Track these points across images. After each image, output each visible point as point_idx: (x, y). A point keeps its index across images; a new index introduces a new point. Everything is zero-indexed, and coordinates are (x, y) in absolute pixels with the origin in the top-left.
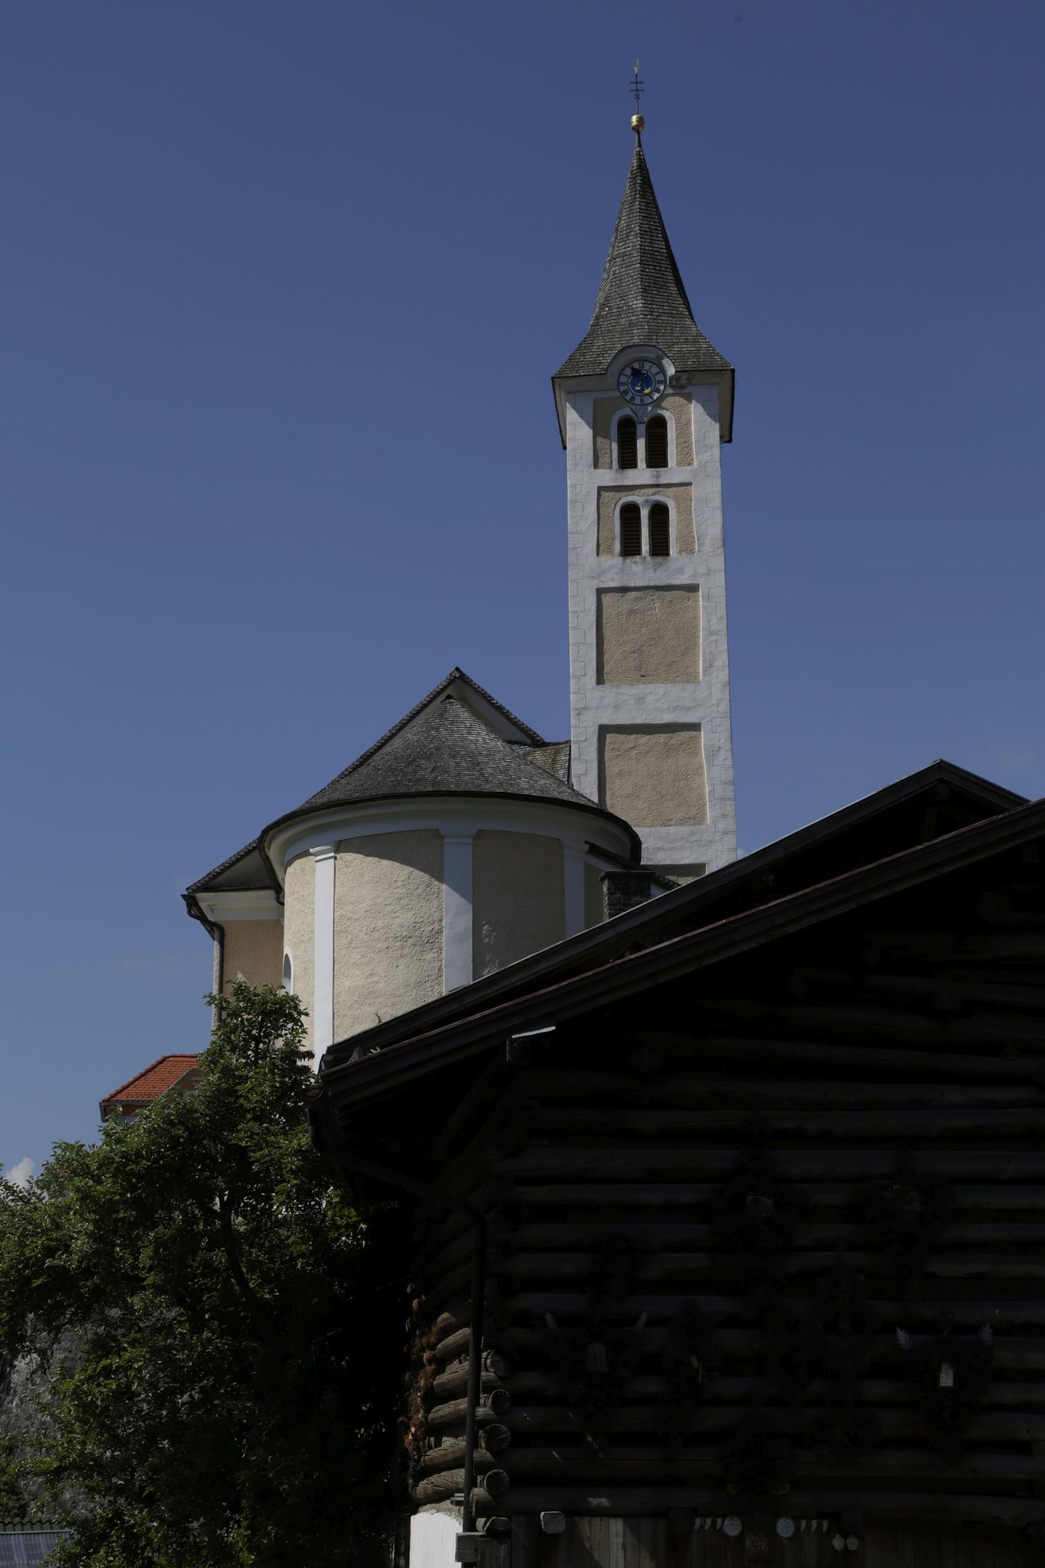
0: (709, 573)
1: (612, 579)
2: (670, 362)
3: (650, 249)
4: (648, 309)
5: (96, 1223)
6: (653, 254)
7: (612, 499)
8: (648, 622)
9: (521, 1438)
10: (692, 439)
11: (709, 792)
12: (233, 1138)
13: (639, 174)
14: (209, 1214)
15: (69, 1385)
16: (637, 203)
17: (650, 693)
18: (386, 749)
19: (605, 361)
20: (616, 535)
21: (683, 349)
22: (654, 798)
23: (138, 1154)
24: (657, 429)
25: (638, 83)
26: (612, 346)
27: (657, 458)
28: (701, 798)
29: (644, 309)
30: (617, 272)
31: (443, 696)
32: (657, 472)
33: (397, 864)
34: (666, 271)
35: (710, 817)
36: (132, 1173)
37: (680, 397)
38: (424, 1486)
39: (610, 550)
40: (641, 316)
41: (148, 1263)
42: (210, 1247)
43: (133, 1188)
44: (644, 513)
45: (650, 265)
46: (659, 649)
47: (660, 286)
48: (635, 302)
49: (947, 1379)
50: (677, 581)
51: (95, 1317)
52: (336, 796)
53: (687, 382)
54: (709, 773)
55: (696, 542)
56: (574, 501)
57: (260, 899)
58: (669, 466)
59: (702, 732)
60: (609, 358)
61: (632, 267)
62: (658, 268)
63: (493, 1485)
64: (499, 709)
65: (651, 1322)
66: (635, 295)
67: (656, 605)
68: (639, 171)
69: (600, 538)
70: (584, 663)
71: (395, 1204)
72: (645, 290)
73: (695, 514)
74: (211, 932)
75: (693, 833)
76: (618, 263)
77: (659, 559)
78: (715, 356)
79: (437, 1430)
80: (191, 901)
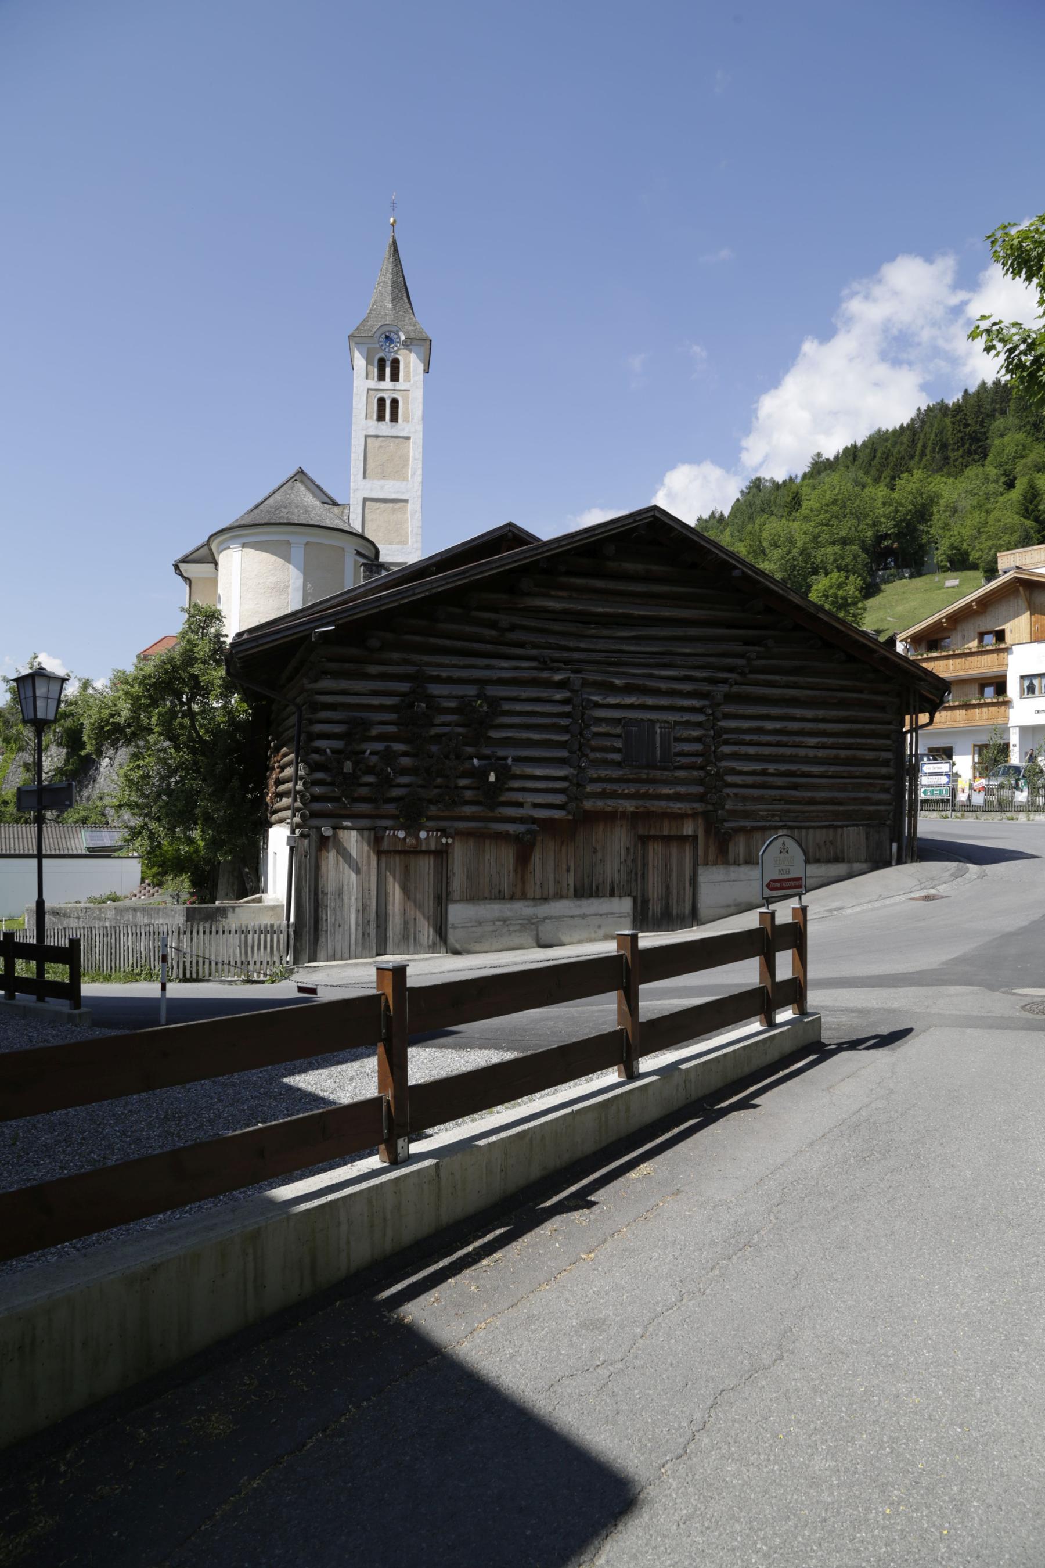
5: (132, 704)
9: (315, 798)
12: (192, 671)
14: (182, 704)
15: (122, 772)
18: (266, 502)
23: (150, 676)
24: (396, 363)
27: (395, 377)
31: (293, 480)
33: (270, 555)
36: (147, 684)
38: (275, 817)
39: (371, 418)
41: (155, 723)
42: (182, 717)
43: (148, 690)
49: (492, 778)
51: (133, 744)
52: (243, 523)
56: (356, 394)
57: (207, 568)
63: (302, 816)
64: (318, 487)
65: (371, 754)
71: (264, 702)
72: (393, 300)
74: (185, 581)
77: (394, 424)
79: (280, 795)
80: (177, 567)
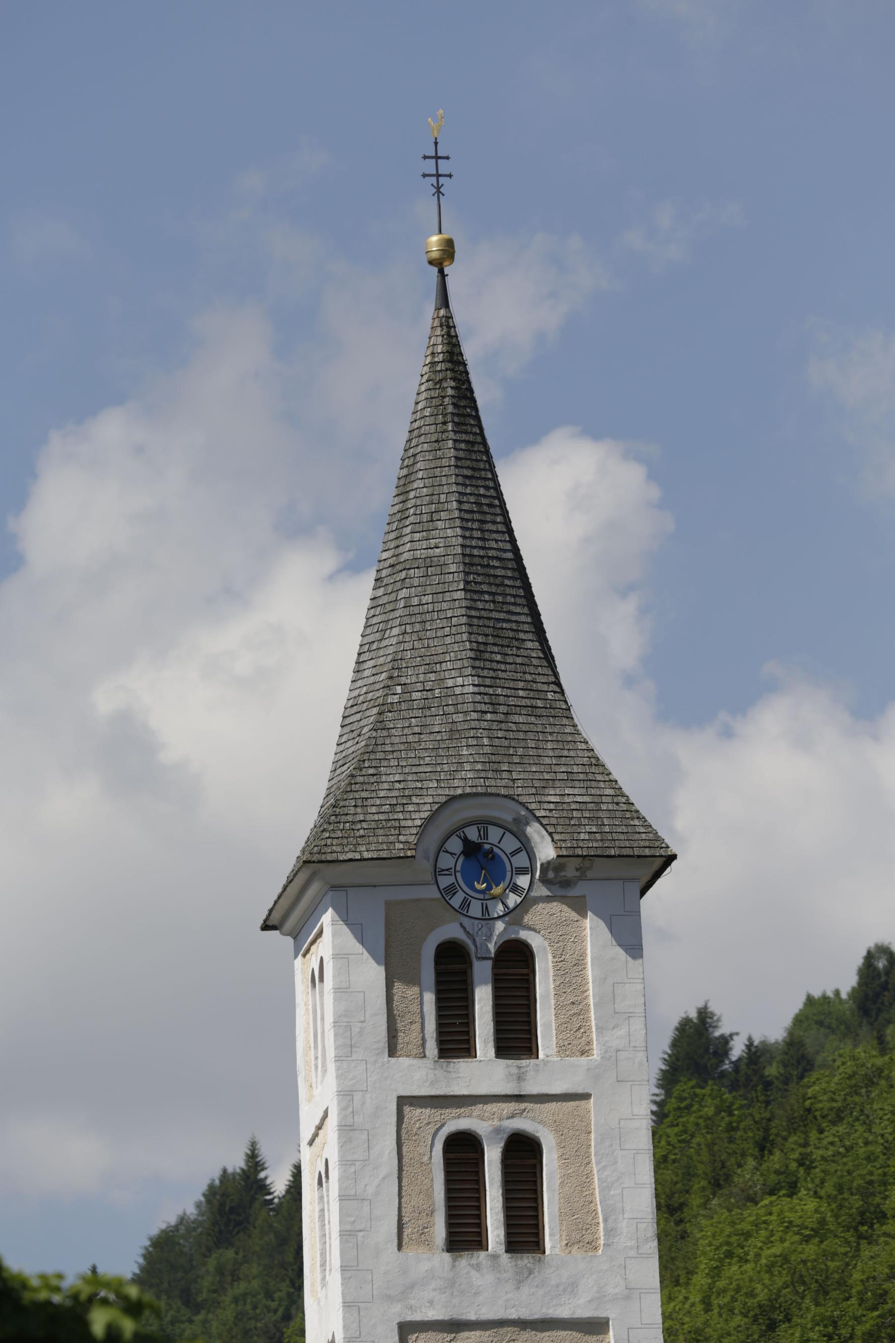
0: (630, 1293)
1: (431, 1302)
2: (544, 832)
3: (482, 553)
6: (488, 566)
7: (429, 1123)
10: (587, 997)
16: (450, 444)
19: (409, 823)
20: (437, 1206)
21: (567, 799)
25: (440, 158)
26: (419, 785)
30: (415, 601)
32: (519, 1068)
34: (515, 604)
37: (563, 903)
40: (474, 716)
44: (492, 1157)
45: (483, 592)
47: (505, 642)
48: (460, 681)
53: (578, 874)
55: (601, 1225)
58: (541, 1054)
61: (447, 597)
62: (500, 599)
66: (458, 664)
68: (449, 365)
69: (404, 1210)
72: (479, 654)
73: (598, 1163)
76: (416, 582)
77: (526, 1260)
78: (632, 819)
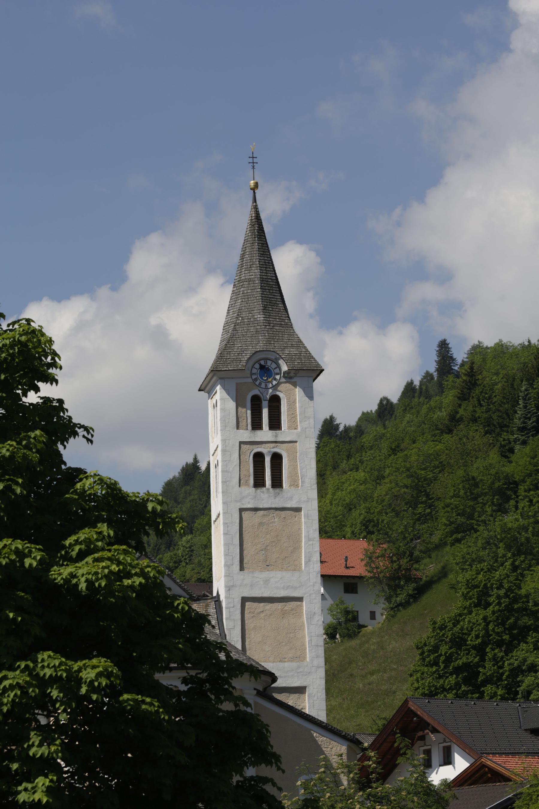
0: (308, 500)
3: (266, 277)
4: (267, 322)
6: (268, 281)
8: (271, 531)
11: (309, 641)
13: (256, 222)
16: (256, 244)
17: (273, 577)
19: (243, 359)
21: (291, 352)
22: (275, 644)
26: (246, 348)
27: (275, 424)
28: (304, 644)
29: (264, 321)
30: (246, 292)
34: (276, 293)
35: (309, 657)
45: (266, 289)
46: (277, 549)
47: (273, 304)
50: (289, 505)
54: (308, 629)
58: (283, 429)
59: (304, 603)
60: (246, 357)
61: (255, 290)
62: (271, 291)
67: (276, 520)
68: (256, 220)
70: (232, 557)
72: (265, 308)
75: (299, 667)
77: (277, 490)
